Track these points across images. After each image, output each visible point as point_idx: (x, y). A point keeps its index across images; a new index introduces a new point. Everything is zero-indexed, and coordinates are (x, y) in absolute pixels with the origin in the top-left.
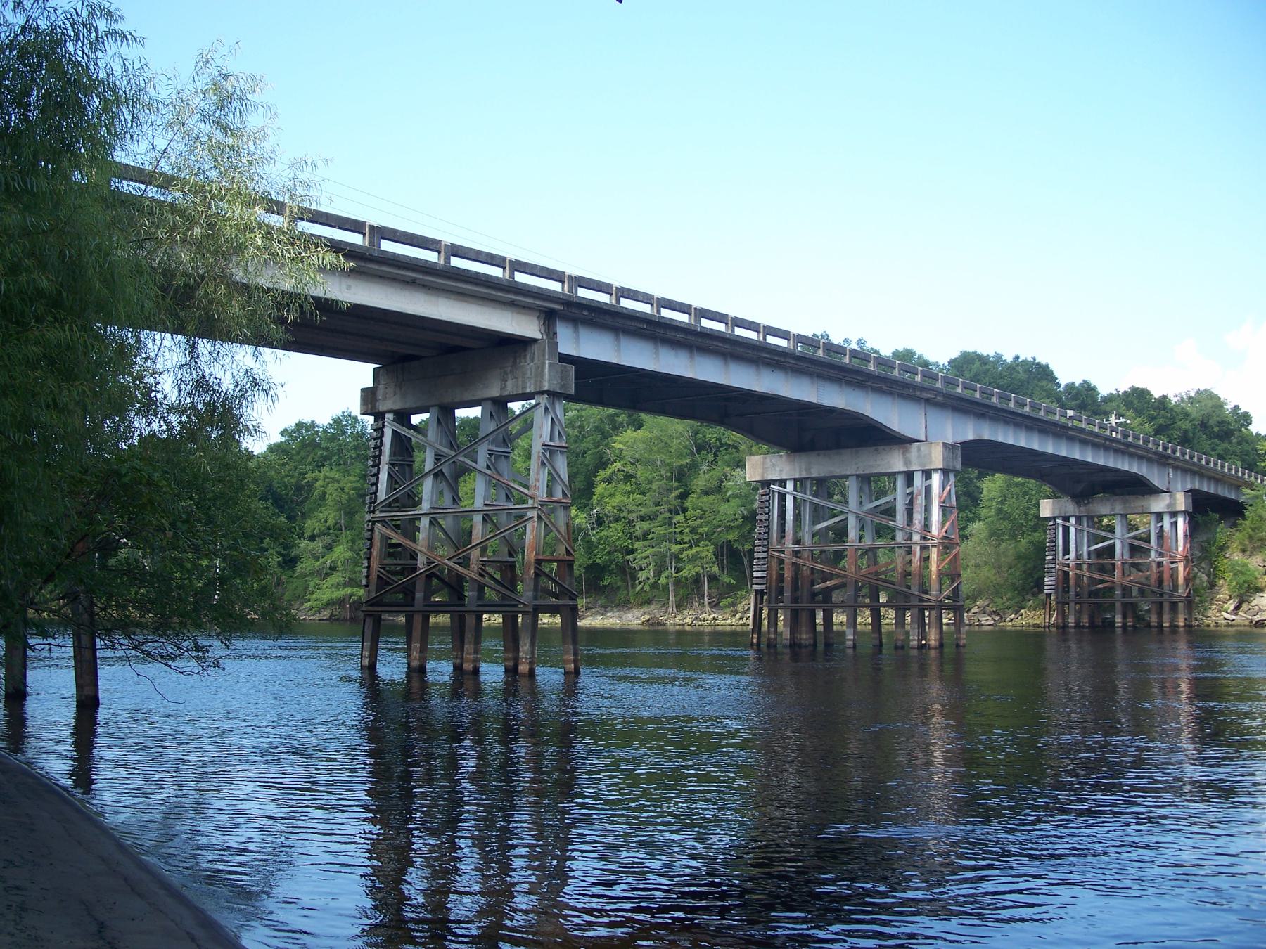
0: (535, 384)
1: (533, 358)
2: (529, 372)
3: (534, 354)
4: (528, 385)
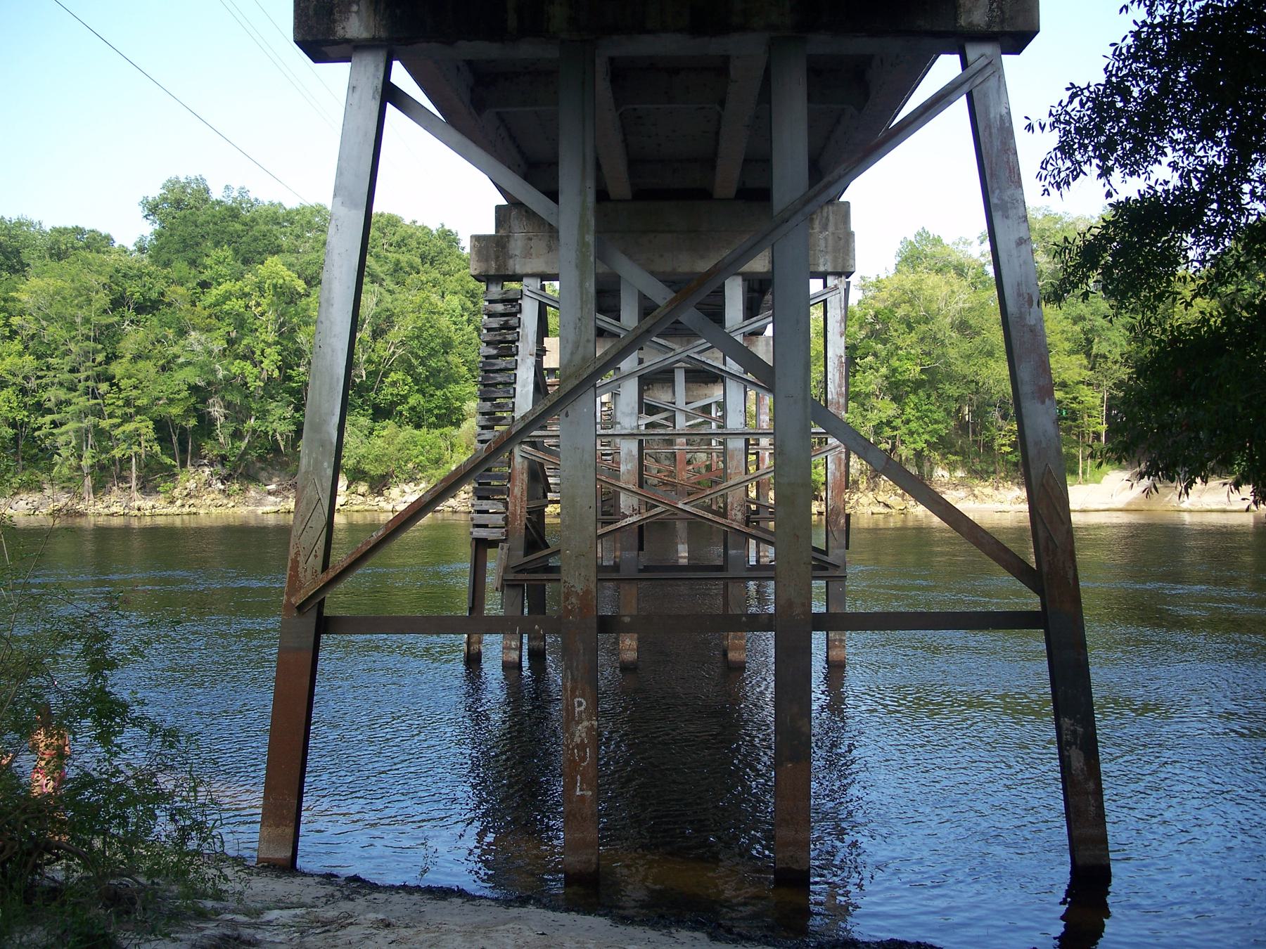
0: (835, 260)
1: (827, 225)
2: (822, 243)
3: (827, 218)
4: (821, 261)
